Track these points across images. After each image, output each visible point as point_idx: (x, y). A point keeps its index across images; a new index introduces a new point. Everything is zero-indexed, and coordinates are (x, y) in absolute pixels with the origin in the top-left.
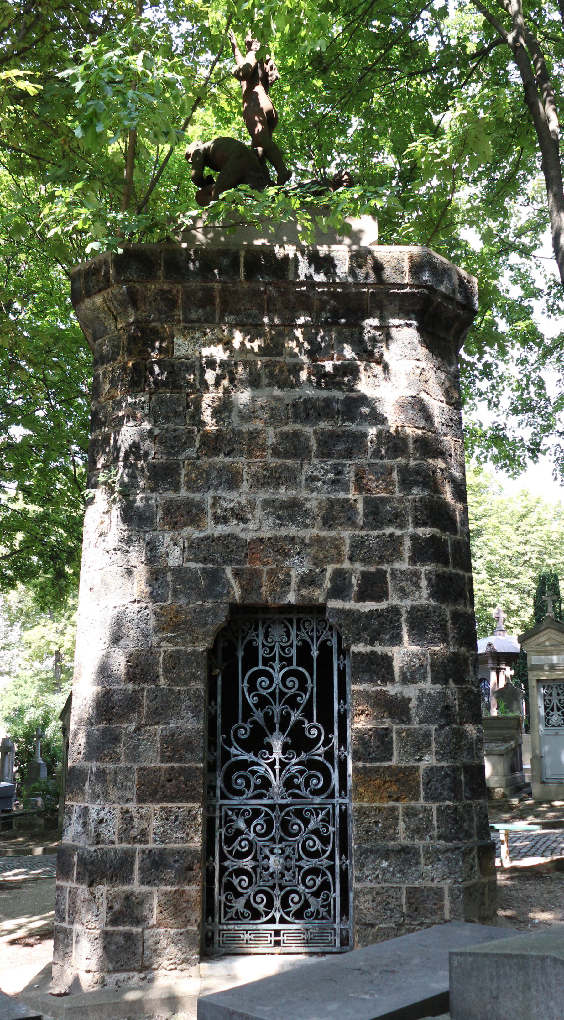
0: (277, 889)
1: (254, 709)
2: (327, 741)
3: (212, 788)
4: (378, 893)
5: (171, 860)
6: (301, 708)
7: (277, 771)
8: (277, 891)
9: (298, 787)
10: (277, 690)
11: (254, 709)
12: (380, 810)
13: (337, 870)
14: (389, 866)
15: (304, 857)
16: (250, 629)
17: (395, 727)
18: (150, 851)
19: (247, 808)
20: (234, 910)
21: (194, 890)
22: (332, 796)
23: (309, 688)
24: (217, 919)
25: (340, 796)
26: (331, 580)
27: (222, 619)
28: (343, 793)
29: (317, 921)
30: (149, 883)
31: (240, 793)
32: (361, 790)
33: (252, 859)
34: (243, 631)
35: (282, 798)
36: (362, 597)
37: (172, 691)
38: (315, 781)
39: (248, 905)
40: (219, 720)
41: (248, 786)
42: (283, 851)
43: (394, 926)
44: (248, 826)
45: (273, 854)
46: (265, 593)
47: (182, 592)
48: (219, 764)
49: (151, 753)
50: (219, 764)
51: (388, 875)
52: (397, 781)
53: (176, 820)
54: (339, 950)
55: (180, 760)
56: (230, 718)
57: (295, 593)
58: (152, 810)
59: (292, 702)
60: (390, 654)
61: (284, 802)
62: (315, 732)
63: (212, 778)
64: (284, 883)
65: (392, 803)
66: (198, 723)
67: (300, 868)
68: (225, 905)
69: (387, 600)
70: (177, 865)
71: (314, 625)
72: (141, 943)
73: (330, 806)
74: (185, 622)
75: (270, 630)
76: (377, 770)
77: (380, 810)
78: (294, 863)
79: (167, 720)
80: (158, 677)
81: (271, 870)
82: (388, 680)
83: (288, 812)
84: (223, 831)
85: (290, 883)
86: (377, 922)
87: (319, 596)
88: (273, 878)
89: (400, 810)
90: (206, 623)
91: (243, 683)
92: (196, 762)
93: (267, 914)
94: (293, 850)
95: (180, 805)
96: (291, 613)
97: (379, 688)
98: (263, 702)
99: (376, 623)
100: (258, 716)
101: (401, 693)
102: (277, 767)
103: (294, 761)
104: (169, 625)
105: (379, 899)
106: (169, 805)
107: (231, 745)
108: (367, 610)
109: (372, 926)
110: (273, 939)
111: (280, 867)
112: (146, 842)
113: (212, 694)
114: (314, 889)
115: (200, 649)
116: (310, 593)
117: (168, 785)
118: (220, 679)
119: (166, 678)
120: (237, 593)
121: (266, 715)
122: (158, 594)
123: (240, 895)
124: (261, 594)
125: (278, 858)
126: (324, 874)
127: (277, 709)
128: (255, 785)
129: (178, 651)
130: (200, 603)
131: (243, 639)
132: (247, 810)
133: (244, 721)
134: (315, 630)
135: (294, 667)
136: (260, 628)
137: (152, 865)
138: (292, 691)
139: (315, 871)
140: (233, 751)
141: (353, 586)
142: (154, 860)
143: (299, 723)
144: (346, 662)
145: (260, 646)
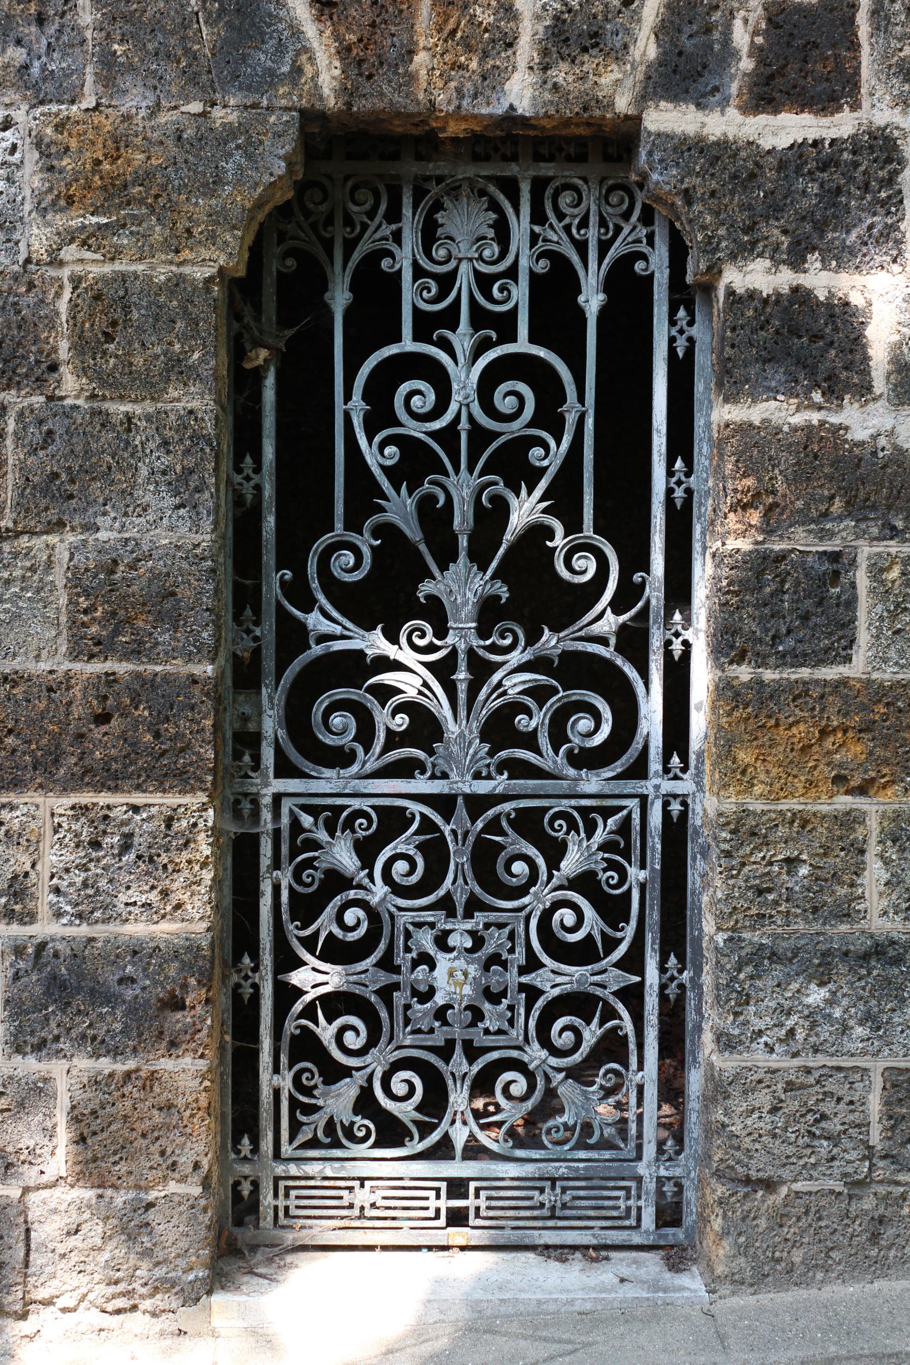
0: (458, 1054)
1: (385, 484)
2: (628, 595)
3: (249, 741)
4: (790, 1086)
5: (111, 977)
6: (543, 485)
7: (462, 688)
8: (459, 1063)
9: (530, 741)
10: (464, 425)
11: (385, 484)
12: (804, 823)
13: (651, 1002)
14: (831, 1002)
15: (545, 959)
16: (371, 215)
17: (865, 551)
18: (41, 947)
19: (362, 804)
20: (320, 1120)
21: (187, 1072)
22: (638, 770)
23: (571, 420)
24: (267, 1144)
25: (666, 770)
26: (662, 31)
27: (276, 160)
28: (675, 760)
29: (582, 1154)
30: (39, 1047)
31: (340, 758)
32: (744, 756)
33: (379, 964)
34: (349, 221)
35: (477, 776)
36: (765, 97)
37: (104, 419)
38: (585, 724)
39: (365, 1103)
40: (270, 522)
41: (366, 735)
42: (479, 942)
43: (839, 1187)
44: (367, 863)
45: (448, 949)
46: (430, 78)
47: (131, 68)
48: (269, 663)
49: (36, 627)
50: (269, 663)
51: (825, 1031)
52: (866, 728)
53: (126, 847)
54: (650, 1240)
55: (135, 652)
56: (304, 515)
57: (531, 78)
58: (44, 813)
59: (515, 467)
60: (856, 299)
61: (483, 787)
62: (588, 566)
63: (247, 709)
64: (481, 1040)
65: (844, 802)
66: (196, 528)
67: (532, 993)
68: (294, 1104)
69: (856, 106)
70: (129, 993)
71: (591, 203)
72: (19, 1232)
73: (633, 803)
74: (144, 178)
75: (440, 217)
76: (800, 692)
77: (804, 823)
78: (513, 978)
79: (88, 517)
80: (54, 368)
81: (440, 999)
82: (848, 387)
83: (497, 818)
84: (286, 878)
85: (501, 1040)
86: (786, 1173)
87: (617, 87)
88: (445, 1023)
89: (873, 824)
90: (219, 181)
91: (348, 397)
92: (190, 658)
93: (425, 1130)
94: (512, 936)
95: (138, 799)
96: (514, 158)
97: (815, 417)
98: (416, 463)
99: (813, 188)
100: (400, 508)
101: (891, 433)
102: (462, 675)
103: (516, 658)
104: (88, 187)
105: (792, 1105)
106: (104, 799)
107: (308, 604)
108: (783, 142)
109: (769, 1185)
110: (444, 1204)
111: (467, 990)
112: (30, 917)
113: (245, 439)
114: (577, 1057)
115: (200, 273)
116: (583, 78)
117: (97, 732)
118: (270, 381)
119: (83, 371)
120: (327, 75)
121: (426, 505)
122: (47, 75)
123: (341, 1073)
124: (412, 78)
125: (461, 963)
126: (610, 1014)
127: (462, 488)
128: (389, 732)
129: (123, 277)
130: (196, 107)
131: (350, 246)
132: (361, 813)
133: (354, 524)
134: (593, 220)
135: (523, 345)
136: (407, 212)
137: (47, 993)
138: (516, 427)
139: (579, 1004)
140: (315, 621)
141: (735, 54)
142: (54, 977)
143: (537, 534)
144: (694, 331)
145: (407, 275)
